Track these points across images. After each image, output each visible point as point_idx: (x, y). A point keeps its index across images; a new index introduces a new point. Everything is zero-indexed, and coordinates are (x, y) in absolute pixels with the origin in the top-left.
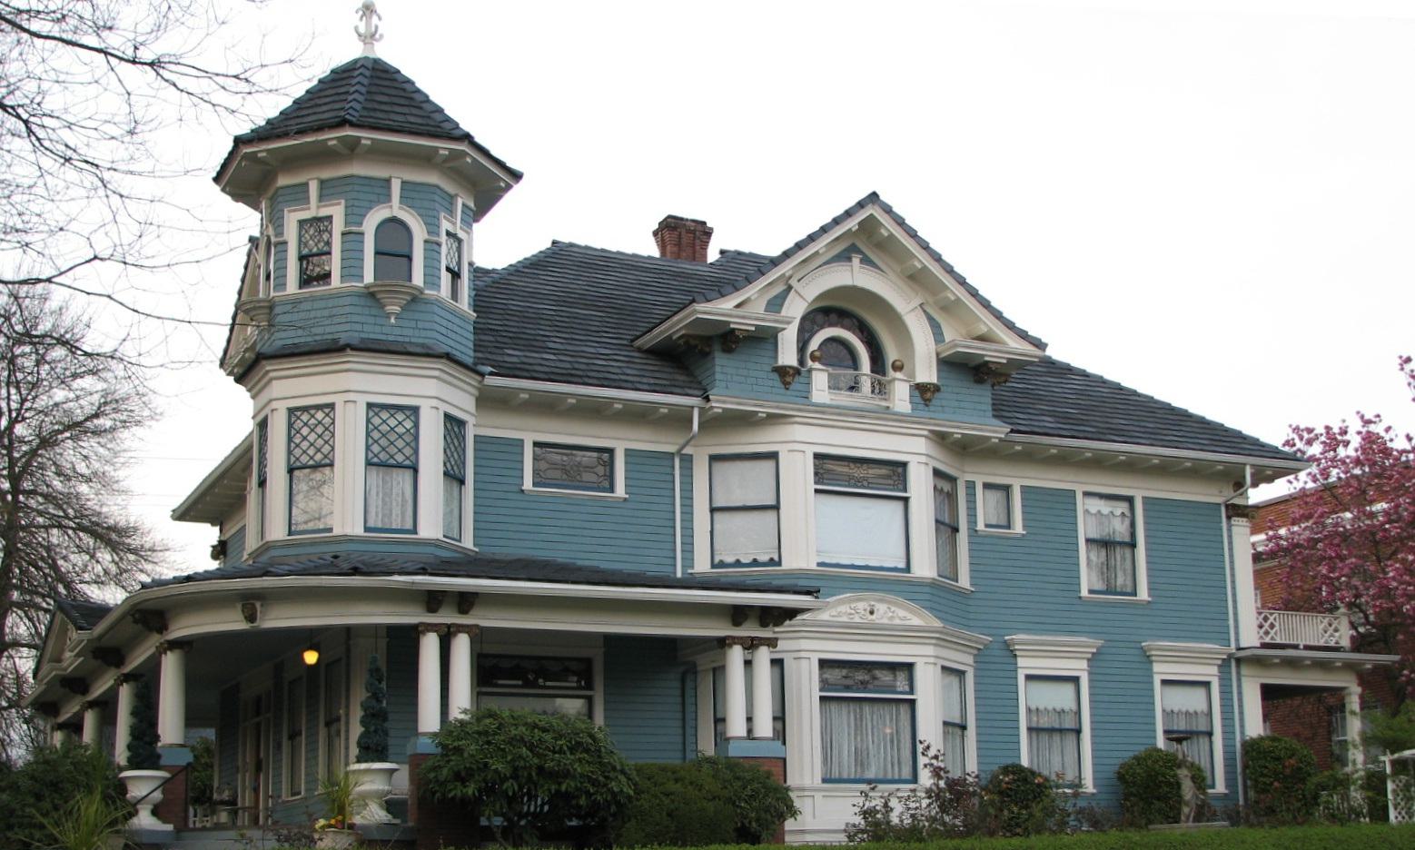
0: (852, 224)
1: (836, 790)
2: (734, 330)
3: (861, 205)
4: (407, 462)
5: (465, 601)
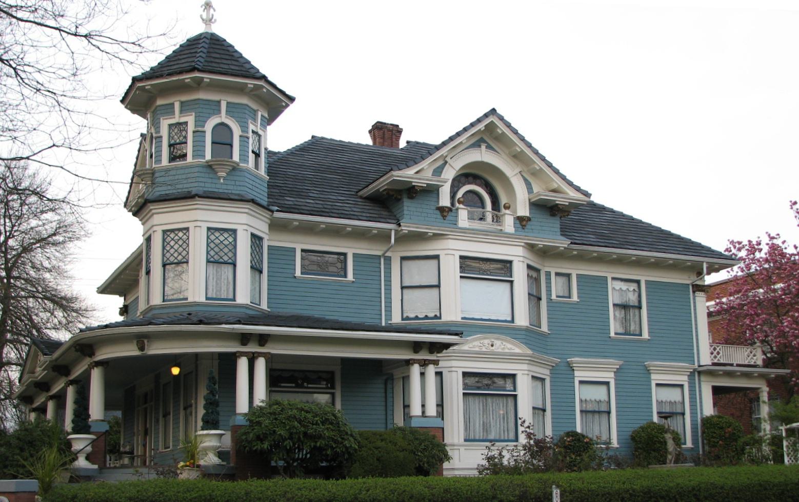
0: (481, 126)
3: (486, 116)
4: (230, 261)
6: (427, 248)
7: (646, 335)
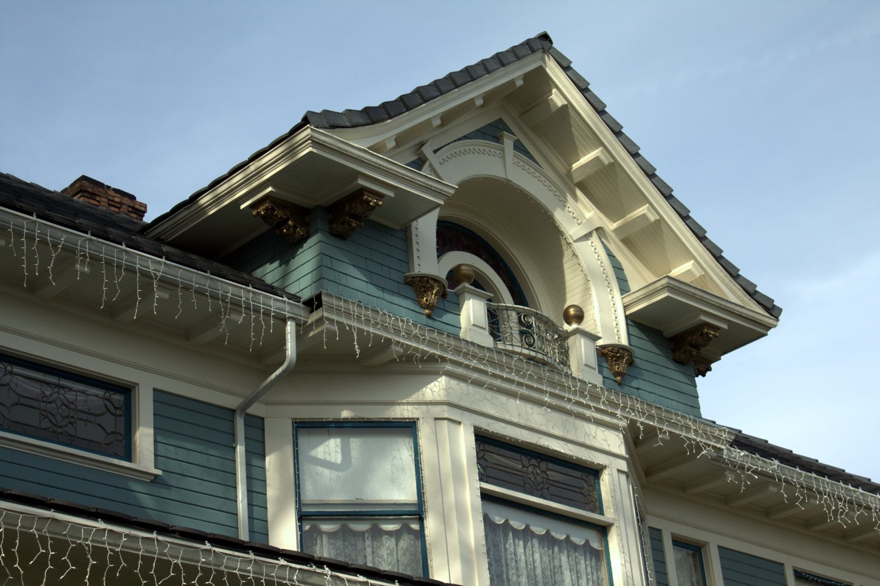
0: (515, 73)
2: (363, 190)
3: (516, 54)
6: (435, 367)
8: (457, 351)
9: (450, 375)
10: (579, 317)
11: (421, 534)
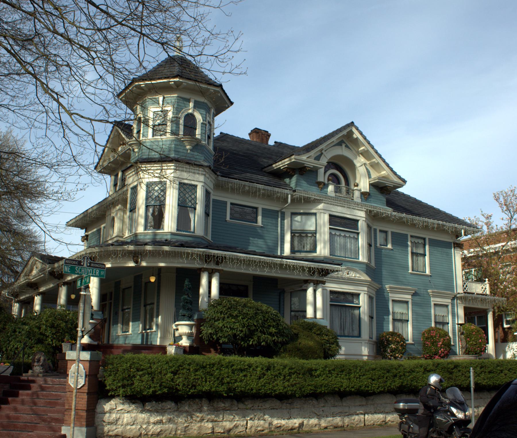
0: (345, 132)
1: (350, 340)
2: (305, 167)
4: (193, 206)
5: (219, 260)
7: (428, 272)
8: (326, 198)
9: (325, 203)
10: (357, 186)
11: (315, 237)
